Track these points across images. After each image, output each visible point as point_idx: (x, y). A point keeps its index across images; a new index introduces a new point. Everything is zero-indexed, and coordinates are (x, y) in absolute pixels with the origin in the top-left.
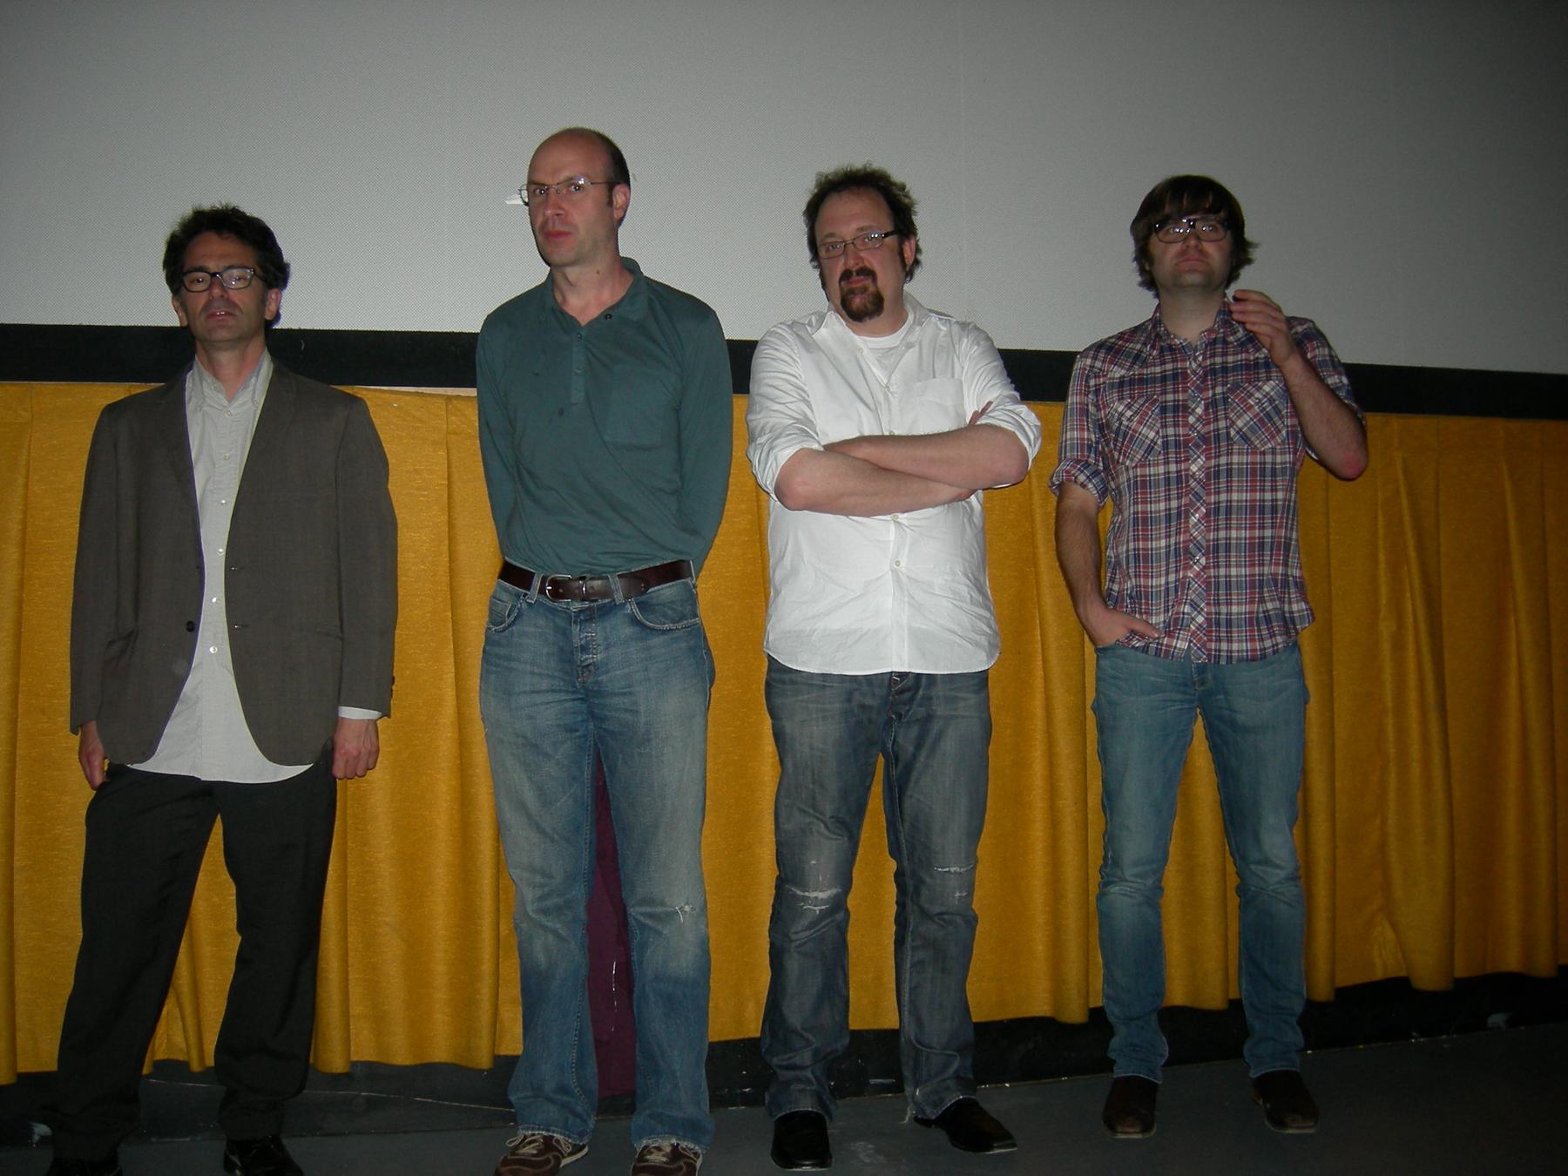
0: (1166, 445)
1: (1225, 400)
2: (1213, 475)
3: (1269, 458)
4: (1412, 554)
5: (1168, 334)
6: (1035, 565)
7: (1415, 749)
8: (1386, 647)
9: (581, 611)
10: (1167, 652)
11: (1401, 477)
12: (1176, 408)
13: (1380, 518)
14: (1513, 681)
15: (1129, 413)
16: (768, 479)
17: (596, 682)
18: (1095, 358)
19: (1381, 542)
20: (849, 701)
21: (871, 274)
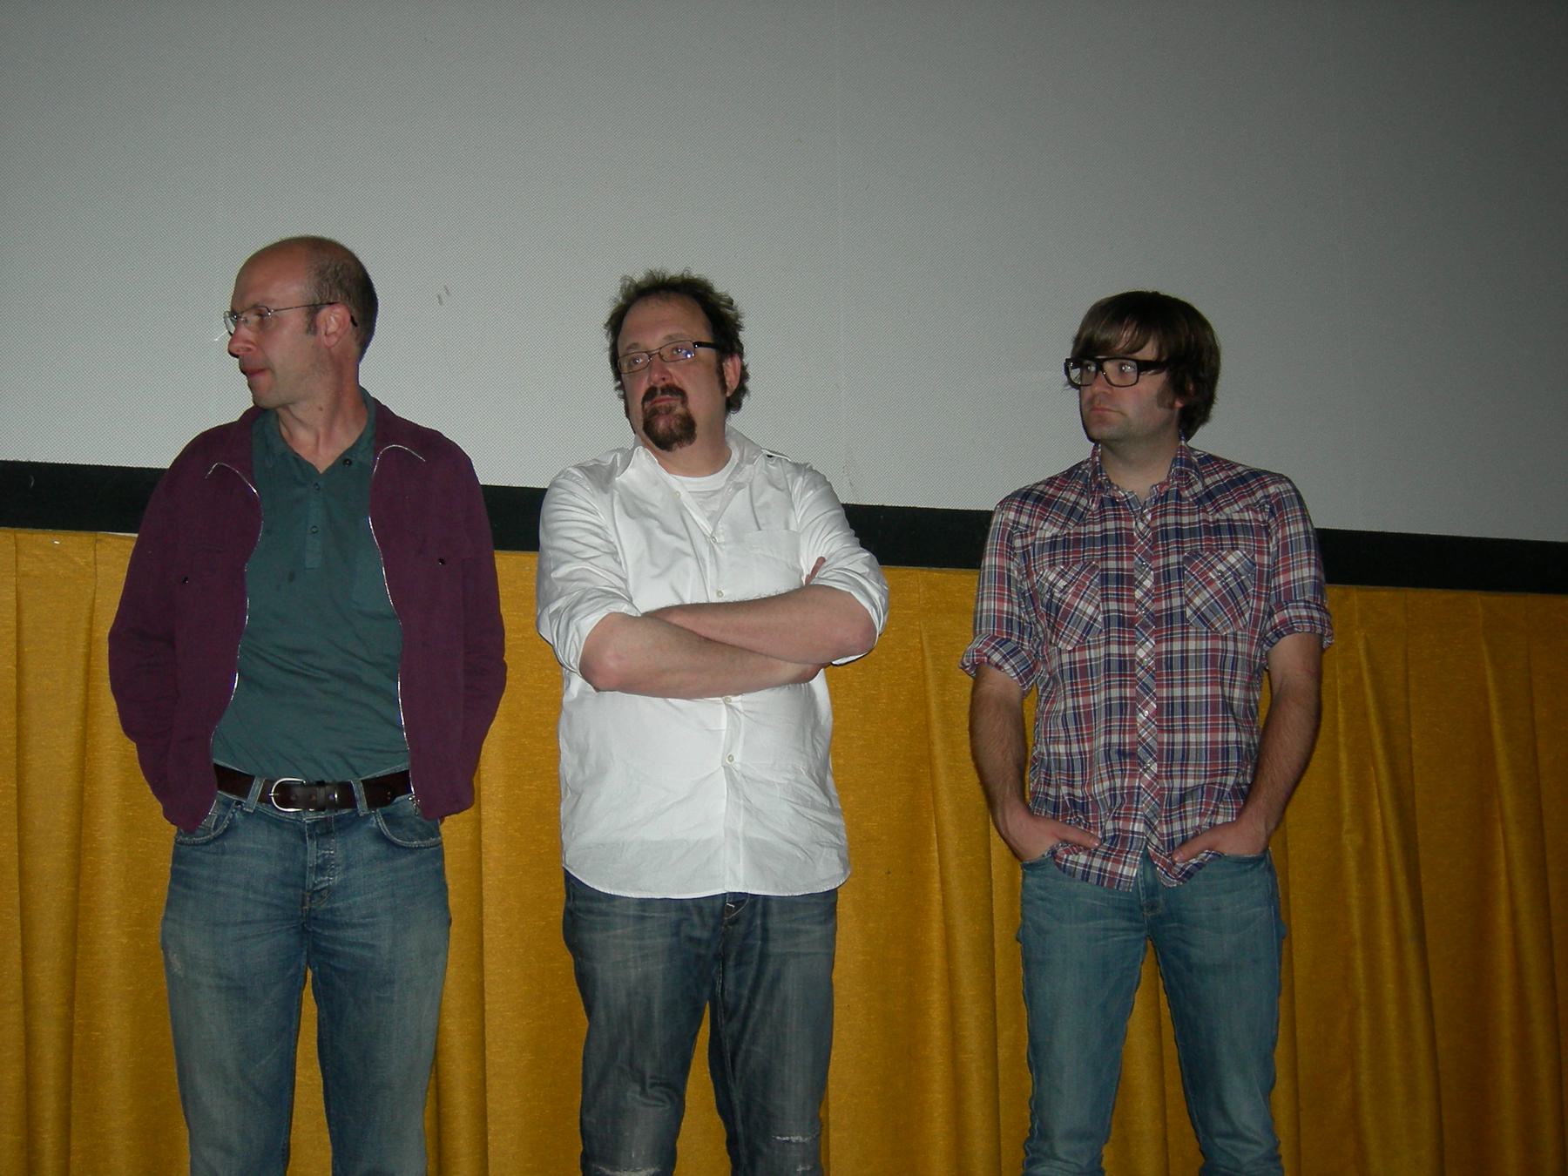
0: (1107, 621)
1: (1180, 571)
2: (1164, 663)
3: (1231, 646)
4: (1379, 751)
5: (1111, 484)
6: (931, 765)
7: (1390, 989)
8: (1351, 865)
9: (316, 823)
10: (1111, 880)
11: (1363, 660)
12: (1119, 579)
13: (1340, 709)
14: (1503, 906)
15: (1062, 583)
16: (571, 654)
17: (332, 911)
18: (1019, 512)
19: (1341, 739)
20: (677, 934)
21: (680, 393)
